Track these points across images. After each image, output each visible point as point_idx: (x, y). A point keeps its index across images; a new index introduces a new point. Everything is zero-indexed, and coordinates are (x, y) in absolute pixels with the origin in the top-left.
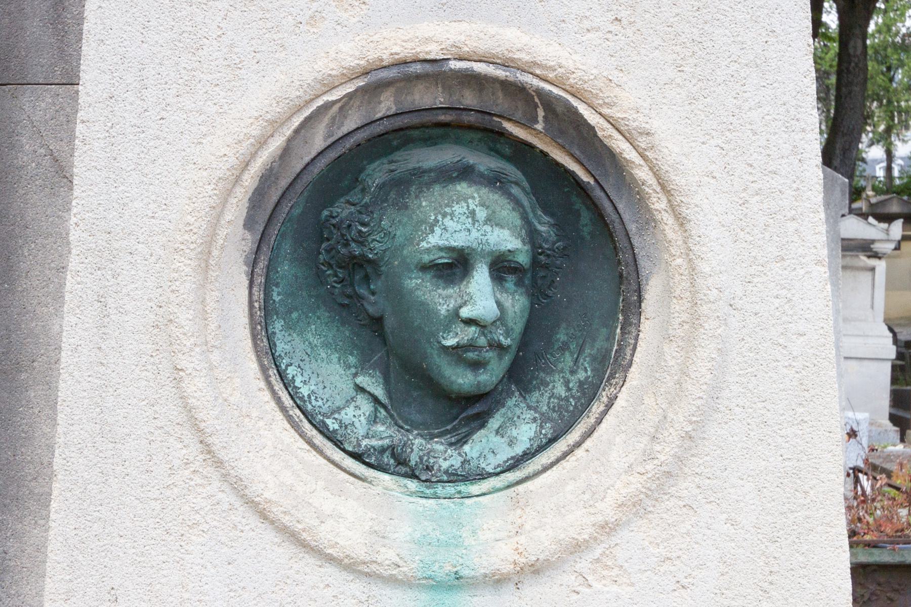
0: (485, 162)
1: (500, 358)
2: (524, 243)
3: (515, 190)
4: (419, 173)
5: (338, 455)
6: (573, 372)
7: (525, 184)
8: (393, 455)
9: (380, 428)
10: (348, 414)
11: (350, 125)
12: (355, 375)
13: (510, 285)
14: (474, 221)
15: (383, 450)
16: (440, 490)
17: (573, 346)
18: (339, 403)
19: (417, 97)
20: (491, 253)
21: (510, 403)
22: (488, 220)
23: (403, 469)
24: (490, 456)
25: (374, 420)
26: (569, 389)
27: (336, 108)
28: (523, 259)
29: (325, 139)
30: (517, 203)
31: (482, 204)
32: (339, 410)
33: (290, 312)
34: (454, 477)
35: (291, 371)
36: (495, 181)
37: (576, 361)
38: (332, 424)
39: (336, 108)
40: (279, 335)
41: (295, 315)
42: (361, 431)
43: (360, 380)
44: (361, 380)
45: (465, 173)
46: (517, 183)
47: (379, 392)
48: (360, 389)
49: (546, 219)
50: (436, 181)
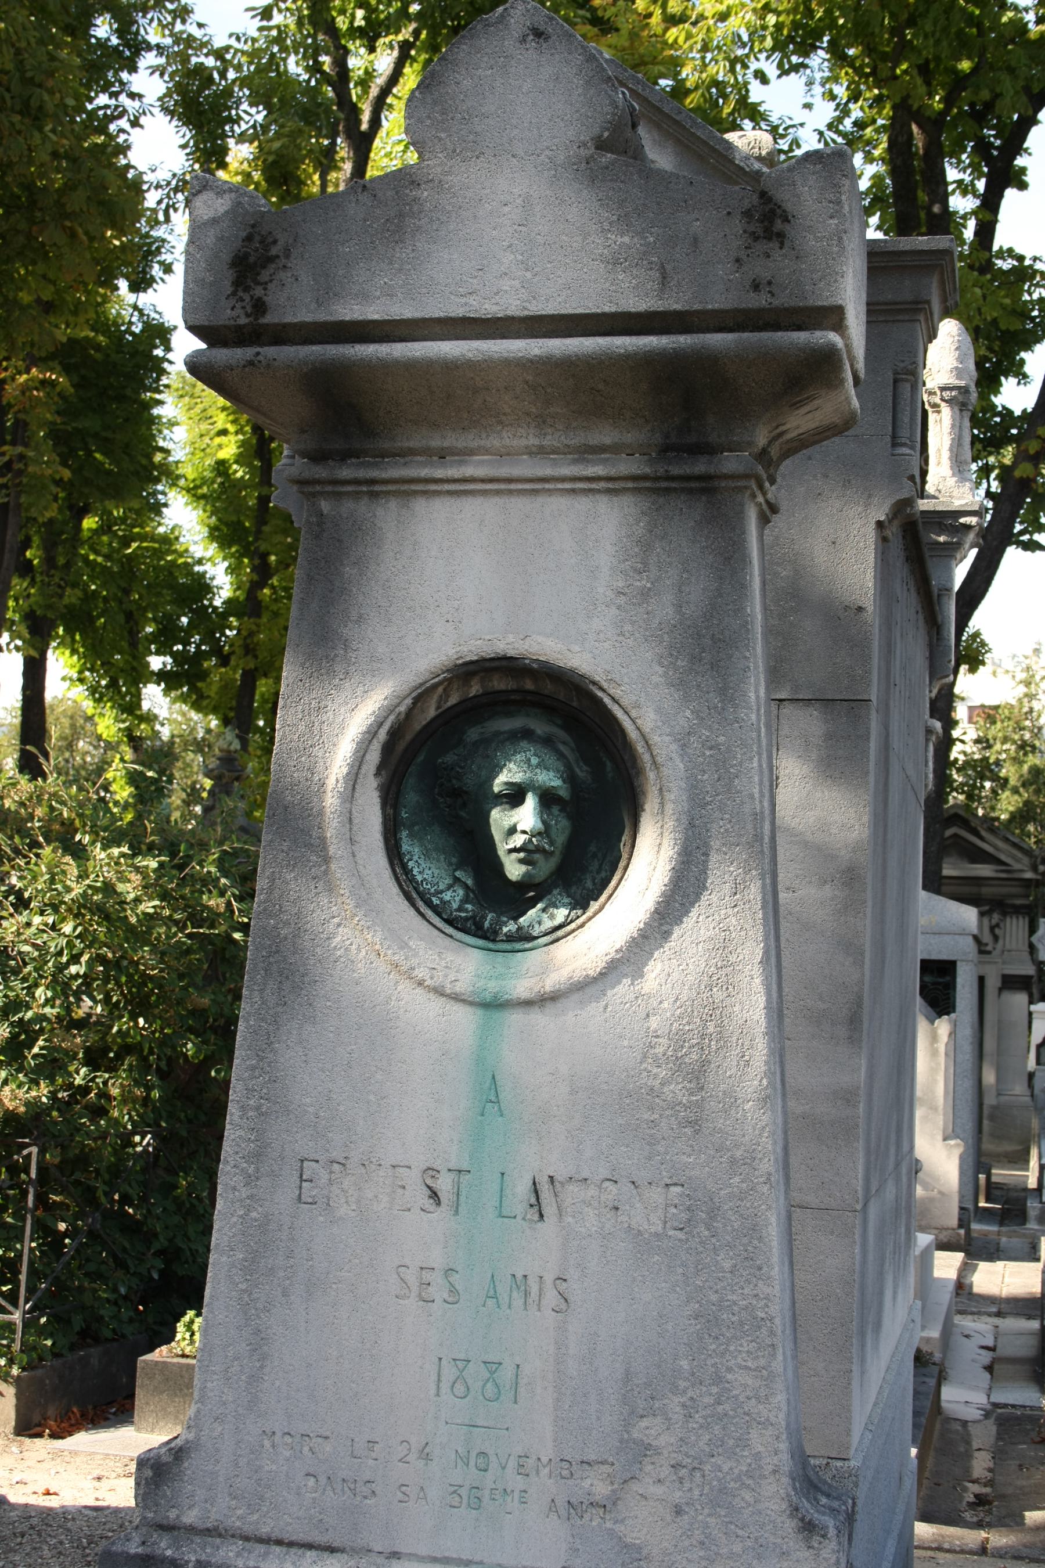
0: (540, 728)
1: (546, 859)
2: (564, 781)
3: (562, 747)
4: (497, 734)
5: (436, 921)
6: (598, 872)
7: (573, 745)
8: (475, 924)
9: (469, 907)
10: (447, 896)
11: (453, 700)
12: (455, 870)
13: (555, 810)
14: (529, 765)
15: (467, 919)
16: (409, 701)
17: (600, 855)
18: (442, 887)
19: (496, 683)
20: (540, 787)
21: (555, 892)
22: (538, 766)
23: (480, 933)
24: (536, 926)
25: (465, 900)
26: (594, 884)
27: (440, 689)
28: (564, 793)
29: (438, 708)
30: (561, 756)
31: (535, 755)
32: (441, 892)
33: (413, 825)
34: (510, 938)
35: (411, 864)
36: (547, 742)
37: (601, 865)
38: (435, 901)
39: (440, 689)
40: (405, 840)
41: (416, 828)
42: (455, 906)
43: (458, 874)
44: (458, 874)
45: (527, 734)
46: (564, 743)
47: (470, 882)
48: (457, 880)
49: (585, 768)
50: (507, 739)
